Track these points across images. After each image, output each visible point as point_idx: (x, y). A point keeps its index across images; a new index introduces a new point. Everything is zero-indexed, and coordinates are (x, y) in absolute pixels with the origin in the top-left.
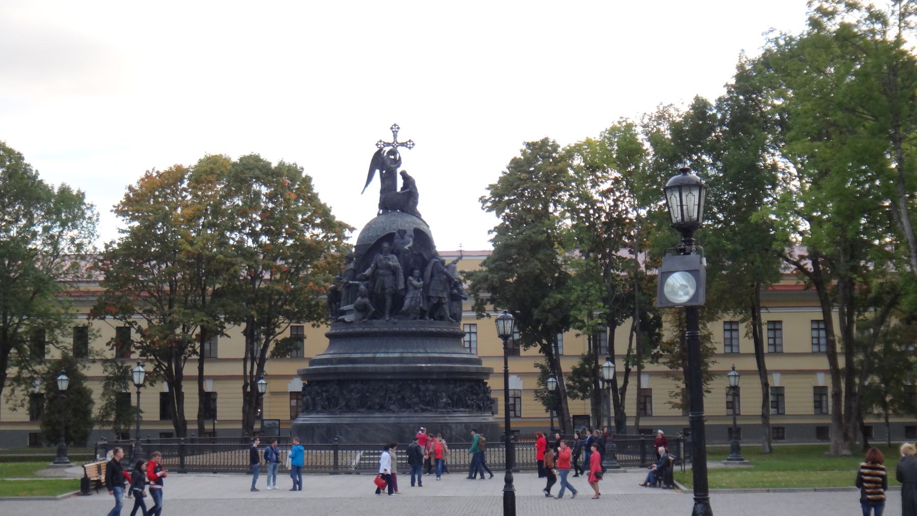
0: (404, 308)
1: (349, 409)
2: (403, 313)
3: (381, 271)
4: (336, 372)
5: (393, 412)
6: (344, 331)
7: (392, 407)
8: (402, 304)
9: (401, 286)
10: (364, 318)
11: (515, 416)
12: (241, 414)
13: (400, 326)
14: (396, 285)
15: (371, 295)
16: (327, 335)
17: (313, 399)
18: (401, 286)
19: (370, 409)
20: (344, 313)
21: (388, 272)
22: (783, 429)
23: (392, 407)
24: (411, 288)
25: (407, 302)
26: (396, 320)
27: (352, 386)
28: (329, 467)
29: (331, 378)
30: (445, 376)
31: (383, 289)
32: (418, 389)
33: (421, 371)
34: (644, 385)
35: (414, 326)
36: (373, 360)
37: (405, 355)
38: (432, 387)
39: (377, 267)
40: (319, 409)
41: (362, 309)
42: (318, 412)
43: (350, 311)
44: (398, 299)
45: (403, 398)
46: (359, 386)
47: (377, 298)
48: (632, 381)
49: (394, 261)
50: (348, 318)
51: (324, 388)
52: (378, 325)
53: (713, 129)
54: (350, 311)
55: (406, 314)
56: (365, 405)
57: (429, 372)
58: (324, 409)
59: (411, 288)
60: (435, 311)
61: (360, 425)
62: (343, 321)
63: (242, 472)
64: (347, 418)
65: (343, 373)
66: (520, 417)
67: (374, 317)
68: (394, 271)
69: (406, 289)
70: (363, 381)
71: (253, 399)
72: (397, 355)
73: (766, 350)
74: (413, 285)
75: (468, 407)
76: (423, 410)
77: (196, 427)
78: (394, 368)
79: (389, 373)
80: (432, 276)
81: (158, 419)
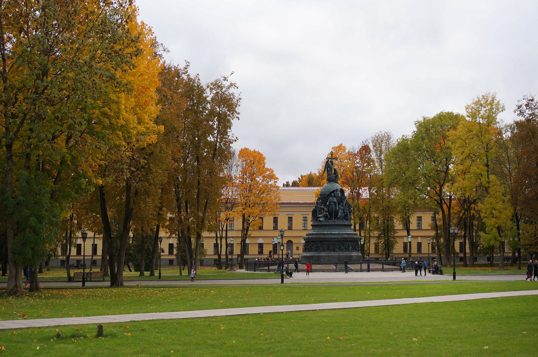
0: (339, 216)
1: (324, 251)
2: (338, 218)
3: (331, 203)
4: (320, 238)
5: (337, 252)
6: (320, 224)
7: (337, 250)
8: (338, 215)
9: (337, 209)
10: (326, 219)
11: (391, 253)
12: (240, 252)
13: (337, 222)
14: (336, 208)
15: (329, 211)
16: (311, 225)
17: (311, 247)
18: (337, 209)
19: (330, 251)
20: (319, 217)
21: (334, 204)
22: (173, 260)
23: (337, 250)
24: (340, 209)
25: (339, 214)
26: (336, 220)
27: (325, 243)
28: (359, 269)
29: (318, 240)
30: (351, 240)
31: (332, 209)
32: (344, 244)
33: (345, 238)
34: (229, 242)
35: (337, 222)
36: (331, 234)
37: (340, 232)
38: (348, 243)
39: (330, 202)
40: (314, 250)
41: (325, 216)
42: (313, 252)
43: (321, 217)
44: (337, 213)
45: (340, 247)
46: (327, 243)
47: (330, 213)
48: (224, 241)
49: (335, 200)
50: (321, 219)
51: (314, 244)
52: (331, 222)
53: (216, 145)
54: (321, 217)
55: (339, 218)
56: (329, 250)
57: (347, 238)
58: (315, 251)
59: (340, 209)
60: (346, 217)
61: (328, 256)
62: (320, 220)
63: (366, 271)
64: (323, 254)
65: (322, 239)
66: (393, 253)
67: (330, 219)
68: (335, 204)
69: (339, 210)
70: (328, 241)
71: (244, 247)
72: (337, 232)
73: (228, 229)
74: (341, 208)
75: (356, 250)
76: (346, 251)
77: (225, 257)
78: (333, 237)
79: (336, 239)
80: (345, 205)
81: (76, 255)
